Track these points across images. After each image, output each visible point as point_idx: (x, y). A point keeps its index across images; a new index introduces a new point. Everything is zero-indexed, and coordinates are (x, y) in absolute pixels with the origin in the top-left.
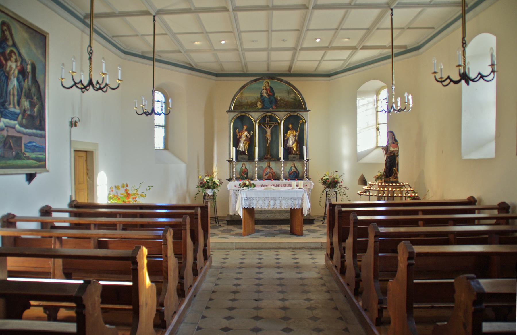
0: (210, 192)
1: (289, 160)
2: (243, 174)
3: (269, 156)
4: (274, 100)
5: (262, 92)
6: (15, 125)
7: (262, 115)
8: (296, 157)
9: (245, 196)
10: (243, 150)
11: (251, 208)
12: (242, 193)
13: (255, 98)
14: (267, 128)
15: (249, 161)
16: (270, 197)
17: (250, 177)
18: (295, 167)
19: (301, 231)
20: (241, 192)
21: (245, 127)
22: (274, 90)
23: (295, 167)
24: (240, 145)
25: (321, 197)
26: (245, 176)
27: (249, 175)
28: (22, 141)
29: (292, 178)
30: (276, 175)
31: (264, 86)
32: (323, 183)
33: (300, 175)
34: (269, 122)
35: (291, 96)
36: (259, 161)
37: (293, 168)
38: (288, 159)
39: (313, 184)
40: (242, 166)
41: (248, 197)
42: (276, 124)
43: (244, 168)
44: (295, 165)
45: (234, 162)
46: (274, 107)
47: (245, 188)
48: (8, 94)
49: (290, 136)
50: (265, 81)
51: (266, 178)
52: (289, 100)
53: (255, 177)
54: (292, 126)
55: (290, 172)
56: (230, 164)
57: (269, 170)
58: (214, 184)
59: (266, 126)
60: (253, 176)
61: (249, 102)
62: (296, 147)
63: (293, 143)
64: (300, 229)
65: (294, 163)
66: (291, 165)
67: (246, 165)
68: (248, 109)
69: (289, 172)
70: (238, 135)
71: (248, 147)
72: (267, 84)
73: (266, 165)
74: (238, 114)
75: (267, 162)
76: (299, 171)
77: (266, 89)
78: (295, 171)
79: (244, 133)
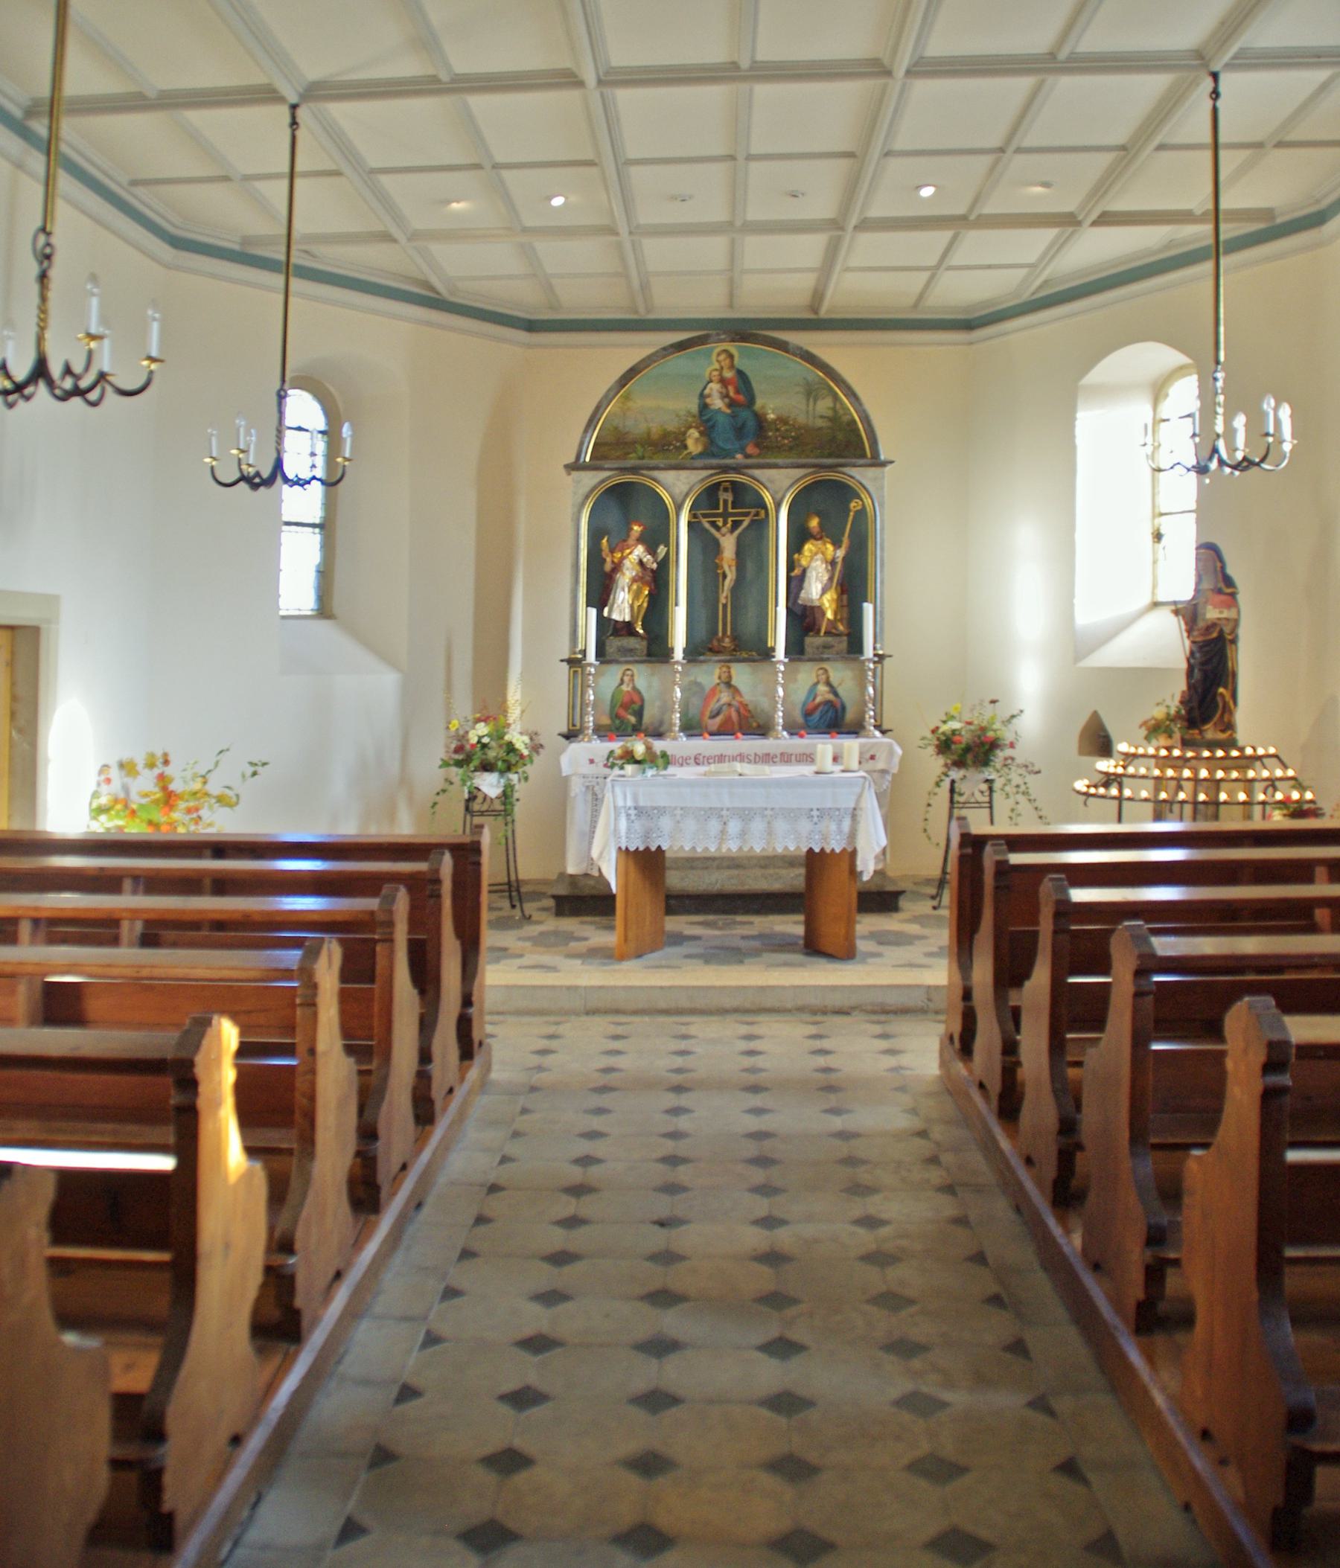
0: (492, 786)
1: (802, 657)
2: (622, 712)
3: (727, 640)
4: (751, 424)
5: (707, 391)
7: (703, 480)
8: (832, 646)
9: (630, 803)
10: (627, 619)
12: (618, 790)
14: (724, 530)
18: (828, 683)
20: (613, 787)
23: (828, 683)
26: (633, 719)
29: (816, 728)
30: (753, 717)
31: (716, 370)
33: (850, 715)
36: (689, 661)
37: (822, 688)
40: (622, 682)
41: (642, 803)
42: (757, 514)
45: (590, 665)
46: (751, 449)
47: (629, 769)
49: (814, 564)
53: (672, 725)
55: (811, 706)
56: (575, 672)
57: (725, 697)
58: (508, 754)
61: (656, 430)
62: (834, 606)
63: (824, 591)
67: (636, 678)
68: (651, 458)
70: (608, 559)
71: (645, 605)
72: (728, 361)
74: (609, 478)
77: (723, 381)
78: (828, 702)
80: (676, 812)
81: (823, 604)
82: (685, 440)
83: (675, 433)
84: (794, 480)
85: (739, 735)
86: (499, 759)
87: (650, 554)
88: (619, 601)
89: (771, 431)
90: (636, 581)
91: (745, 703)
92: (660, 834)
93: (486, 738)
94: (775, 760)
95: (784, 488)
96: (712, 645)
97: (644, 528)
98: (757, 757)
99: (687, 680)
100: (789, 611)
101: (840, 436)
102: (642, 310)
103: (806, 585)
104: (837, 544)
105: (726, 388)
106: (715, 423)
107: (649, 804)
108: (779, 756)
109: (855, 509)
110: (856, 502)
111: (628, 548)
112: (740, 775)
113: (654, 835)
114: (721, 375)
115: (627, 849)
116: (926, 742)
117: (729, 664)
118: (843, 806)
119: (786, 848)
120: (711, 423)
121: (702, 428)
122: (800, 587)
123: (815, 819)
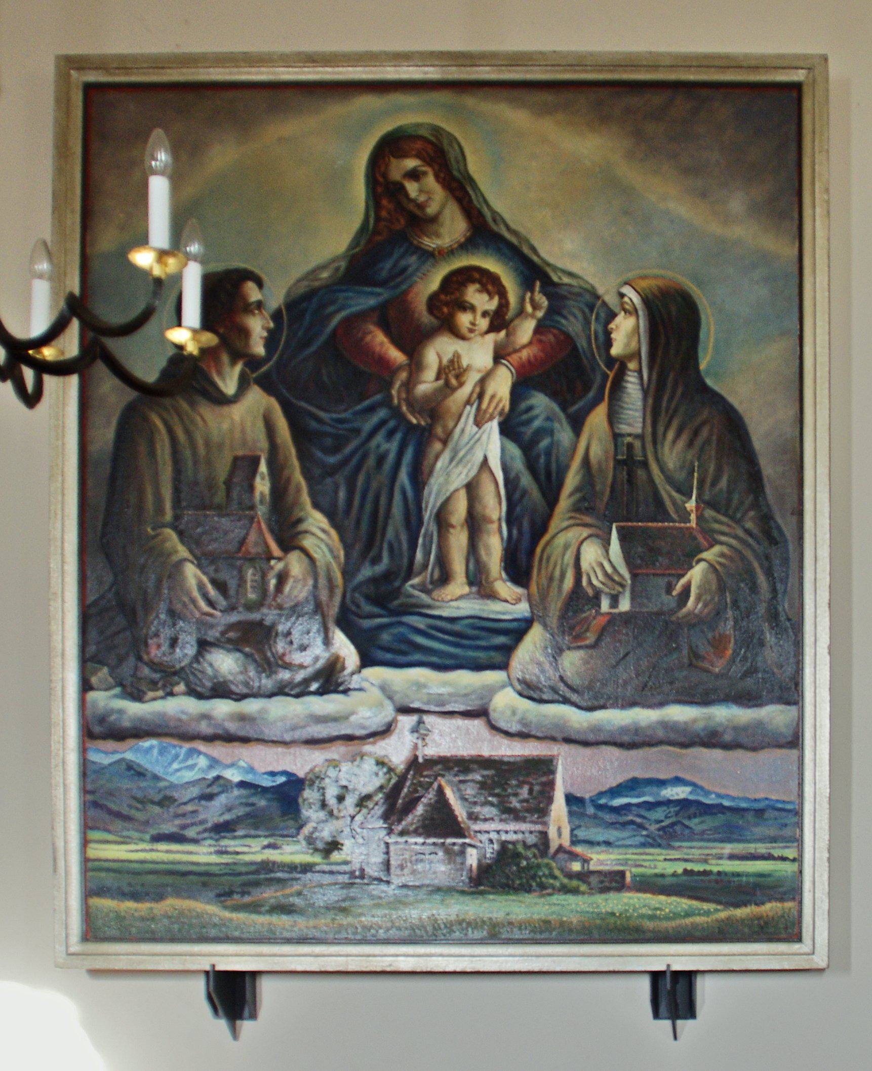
6: (492, 690)
28: (551, 784)
48: (429, 524)
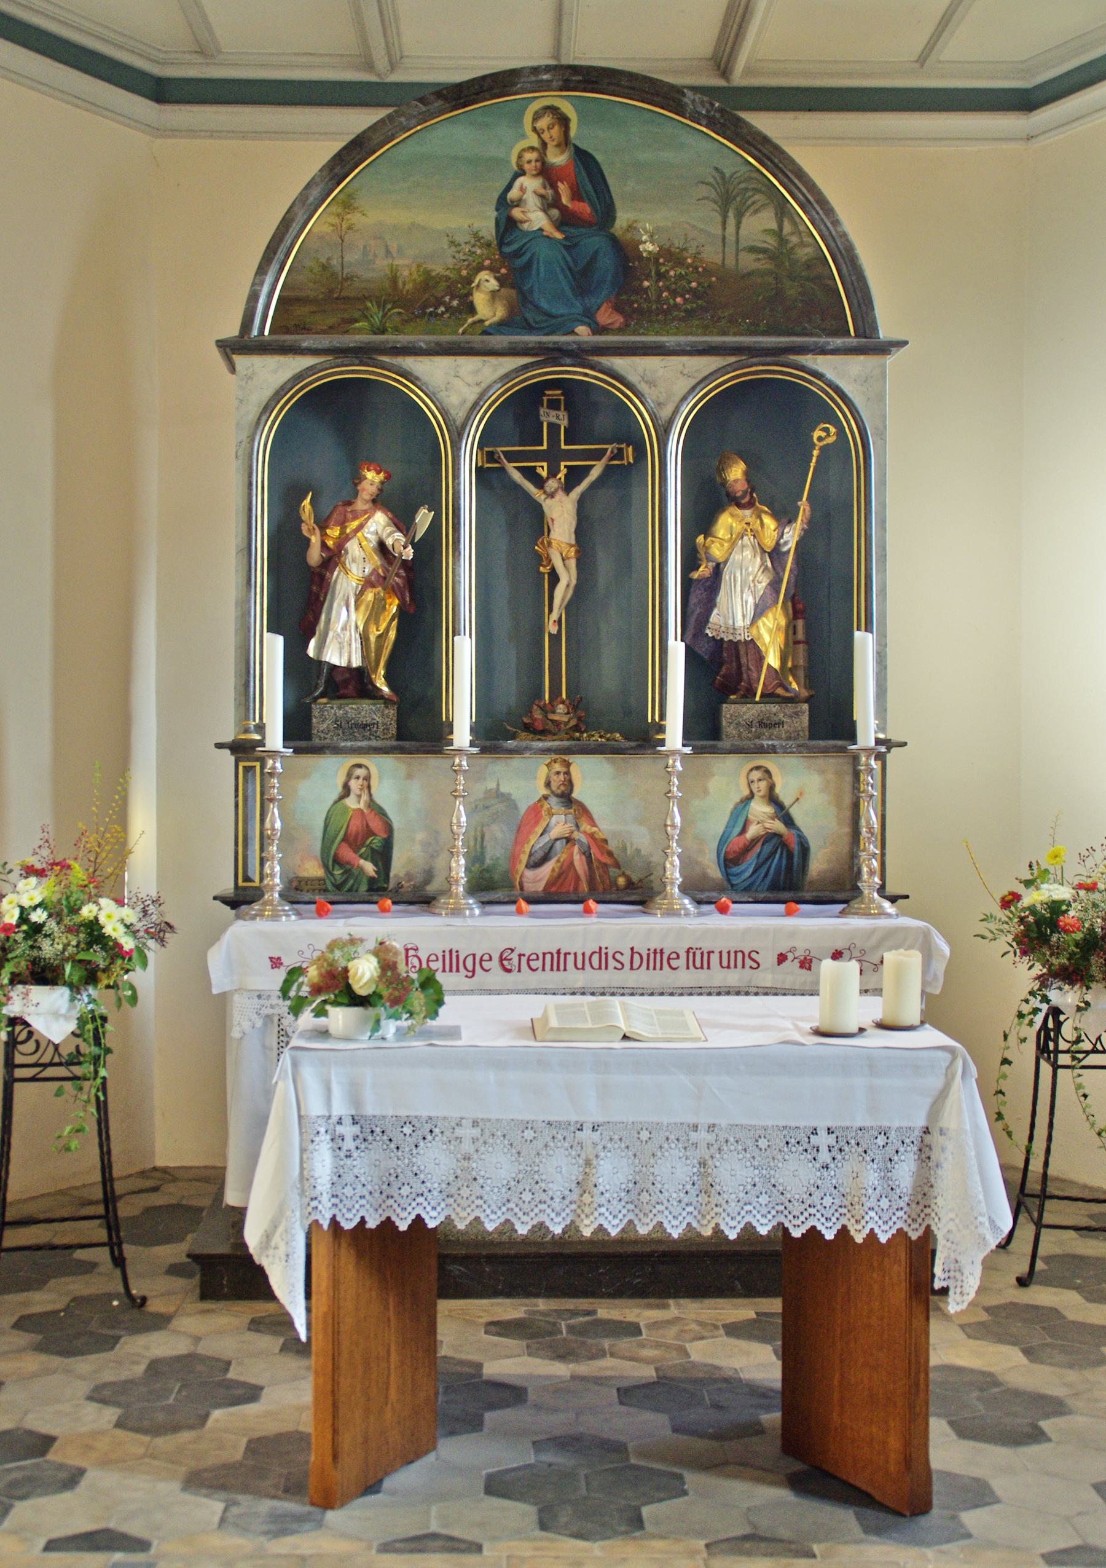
0: (56, 1015)
1: (720, 744)
2: (347, 854)
3: (561, 708)
4: (606, 263)
5: (513, 194)
7: (507, 377)
8: (780, 723)
9: (340, 1108)
10: (356, 662)
11: (403, 1227)
12: (309, 1075)
13: (453, 243)
14: (552, 484)
15: (402, 751)
16: (593, 1113)
17: (409, 876)
18: (772, 799)
19: (907, 1462)
20: (295, 1064)
21: (370, 475)
22: (611, 181)
23: (772, 799)
24: (328, 621)
25: (1005, 1061)
26: (369, 868)
27: (399, 866)
29: (747, 889)
30: (617, 865)
31: (532, 149)
32: (1020, 939)
33: (819, 864)
34: (565, 444)
35: (743, 232)
36: (484, 750)
37: (760, 809)
38: (715, 732)
39: (946, 950)
40: (346, 791)
41: (370, 1110)
42: (620, 454)
43: (362, 806)
44: (772, 787)
45: (274, 754)
46: (606, 316)
47: (340, 1017)
49: (736, 557)
50: (536, 106)
51: (540, 887)
52: (730, 262)
53: (449, 881)
54: (746, 474)
55: (736, 843)
56: (247, 769)
57: (559, 824)
58: (90, 945)
59: (544, 474)
60: (429, 876)
61: (408, 274)
62: (780, 639)
63: (760, 611)
64: (894, 1443)
65: (768, 772)
66: (743, 782)
67: (374, 783)
68: (397, 330)
69: (723, 840)
70: (315, 540)
71: (392, 634)
72: (556, 131)
73: (541, 782)
74: (311, 370)
75: (547, 759)
76: (806, 832)
77: (546, 172)
78: (771, 837)
79: (360, 527)
80: (459, 1132)
81: (760, 636)
82: (470, 294)
83: (448, 278)
84: (693, 382)
85: (592, 904)
86: (67, 960)
87: (400, 530)
88: (337, 626)
89: (648, 277)
90: (373, 586)
91: (601, 836)
92: (418, 1187)
93: (39, 911)
94: (674, 963)
95: (677, 399)
96: (531, 717)
97: (388, 477)
98: (636, 957)
99: (479, 790)
100: (691, 655)
101: (792, 291)
102: (381, 62)
103: (722, 598)
104: (784, 516)
105: (554, 186)
106: (533, 255)
107: (378, 1113)
108: (683, 956)
109: (821, 444)
110: (826, 430)
111: (355, 518)
112: (625, 1037)
113: (405, 1190)
114: (542, 160)
115: (334, 1223)
116: (993, 926)
117: (566, 757)
118: (896, 1124)
119: (749, 1228)
120: (520, 262)
121: (503, 271)
122: (710, 604)
123: (824, 1156)
